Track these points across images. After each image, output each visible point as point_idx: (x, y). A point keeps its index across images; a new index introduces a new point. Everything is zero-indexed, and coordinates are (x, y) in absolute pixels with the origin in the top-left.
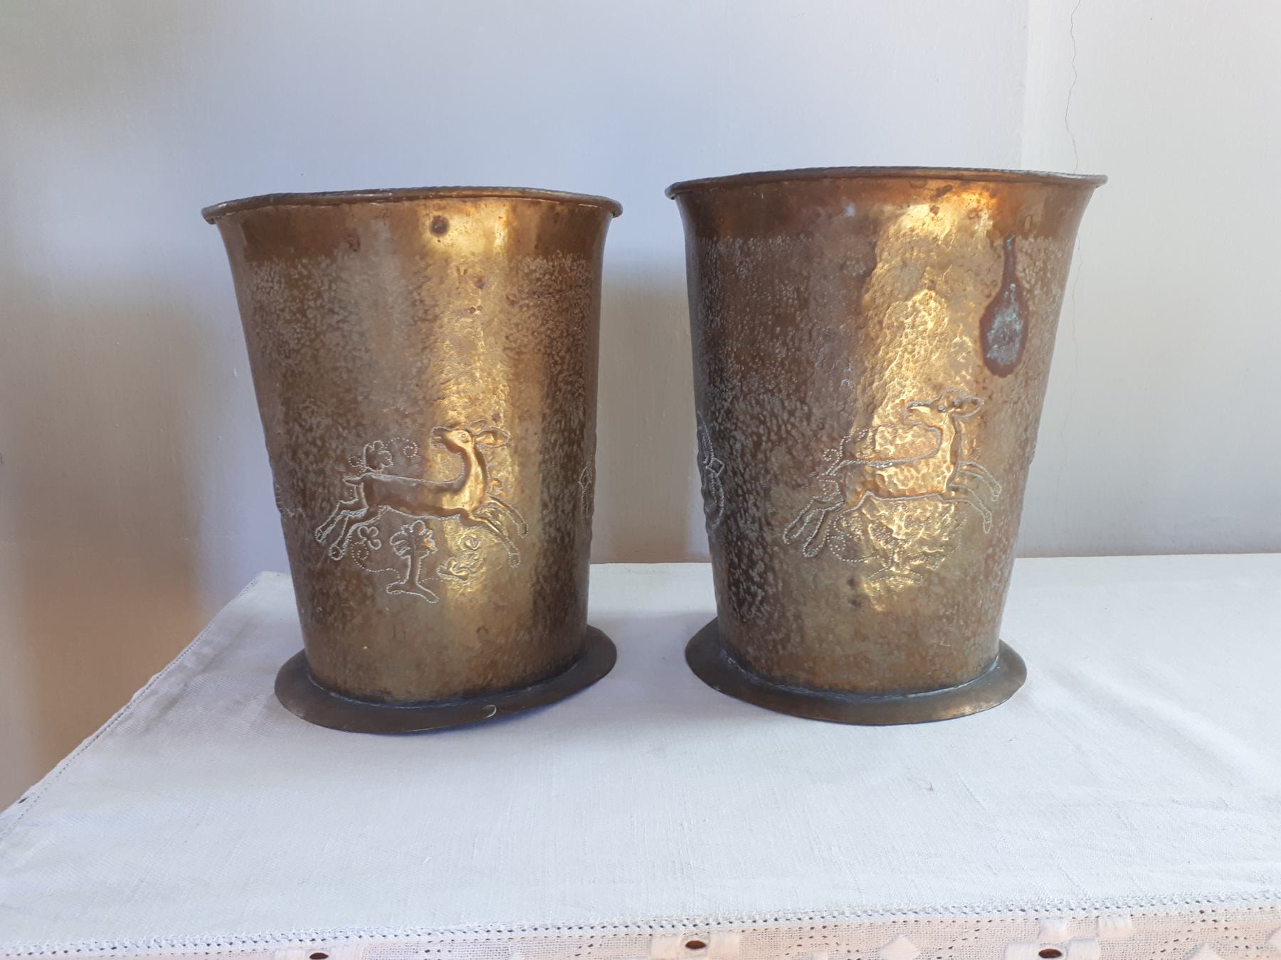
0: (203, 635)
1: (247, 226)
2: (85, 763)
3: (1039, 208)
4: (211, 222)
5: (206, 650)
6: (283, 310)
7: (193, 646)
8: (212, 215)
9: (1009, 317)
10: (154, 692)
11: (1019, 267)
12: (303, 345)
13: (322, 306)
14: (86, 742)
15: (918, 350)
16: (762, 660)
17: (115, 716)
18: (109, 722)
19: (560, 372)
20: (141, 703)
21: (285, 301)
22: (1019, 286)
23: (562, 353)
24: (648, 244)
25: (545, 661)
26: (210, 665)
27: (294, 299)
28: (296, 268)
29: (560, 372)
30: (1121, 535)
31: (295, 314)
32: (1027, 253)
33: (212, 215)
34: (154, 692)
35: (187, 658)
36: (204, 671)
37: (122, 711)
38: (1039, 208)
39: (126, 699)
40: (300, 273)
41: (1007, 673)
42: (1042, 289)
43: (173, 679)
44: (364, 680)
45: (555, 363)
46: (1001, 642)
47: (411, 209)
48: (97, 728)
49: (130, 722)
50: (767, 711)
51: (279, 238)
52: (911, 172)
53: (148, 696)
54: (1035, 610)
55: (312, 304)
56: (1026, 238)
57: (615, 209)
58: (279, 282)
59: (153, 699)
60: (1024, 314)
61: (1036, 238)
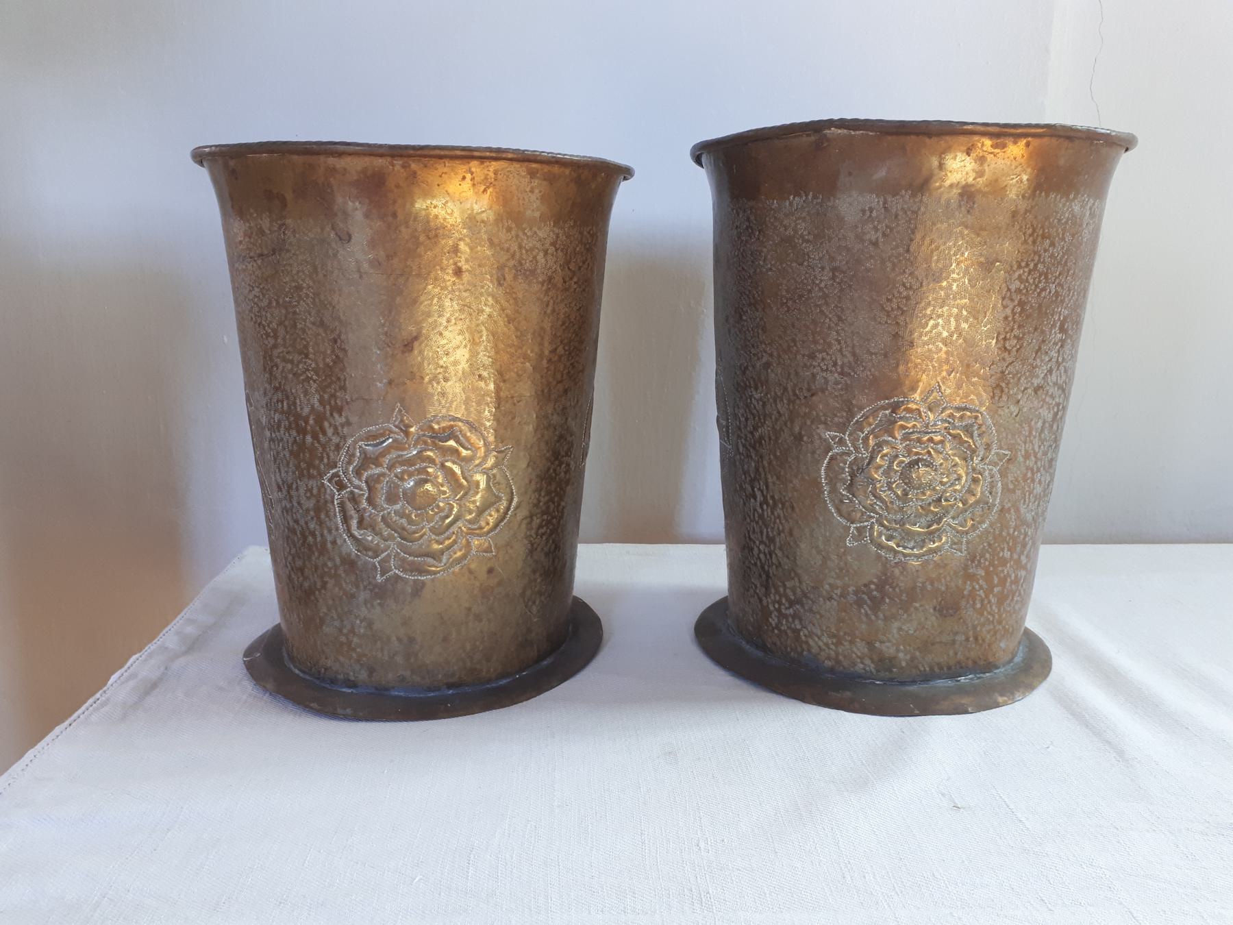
0: (186, 613)
1: (233, 174)
2: (58, 751)
3: (1073, 160)
4: (201, 163)
5: (189, 629)
7: (177, 624)
8: (200, 156)
10: (133, 676)
14: (57, 730)
15: (951, 322)
16: (770, 644)
17: (91, 701)
18: (83, 708)
19: (275, 346)
20: (118, 687)
23: (274, 325)
24: (668, 209)
25: (541, 647)
26: (193, 645)
29: (275, 346)
30: (1125, 526)
33: (200, 156)
34: (133, 676)
35: (169, 638)
36: (185, 653)
37: (98, 695)
38: (1073, 160)
43: (153, 661)
44: (329, 667)
45: (268, 335)
48: (70, 715)
49: (106, 709)
50: (782, 698)
51: (268, 185)
52: (426, 152)
53: (128, 680)
54: (1064, 596)
57: (626, 172)
59: (132, 683)
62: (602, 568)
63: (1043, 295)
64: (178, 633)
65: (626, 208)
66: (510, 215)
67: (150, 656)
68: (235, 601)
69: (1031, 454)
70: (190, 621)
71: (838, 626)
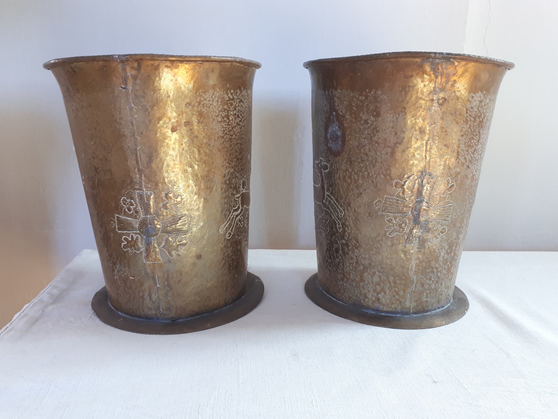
0: (53, 283)
5: (55, 291)
6: (217, 116)
7: (48, 288)
8: (48, 66)
9: (334, 128)
10: (26, 315)
11: (336, 104)
12: (226, 134)
13: (235, 114)
16: (340, 294)
17: (4, 328)
20: (18, 320)
21: (220, 112)
22: (337, 113)
24: (284, 87)
25: (234, 298)
26: (56, 299)
27: (225, 110)
28: (228, 94)
31: (223, 118)
32: (338, 98)
33: (48, 66)
34: (26, 315)
35: (44, 295)
37: (8, 325)
39: (9, 319)
40: (229, 97)
41: (458, 305)
42: (351, 115)
44: (130, 307)
46: (456, 287)
47: (145, 66)
49: (12, 333)
51: (91, 82)
53: (23, 317)
54: (472, 273)
55: (232, 113)
56: (336, 90)
58: (218, 101)
59: (25, 319)
60: (341, 127)
61: (341, 90)
62: (257, 260)
63: (472, 125)
64: (48, 293)
65: (261, 86)
66: (200, 87)
67: (35, 305)
68: (78, 276)
69: (463, 184)
70: (55, 287)
71: (361, 285)
